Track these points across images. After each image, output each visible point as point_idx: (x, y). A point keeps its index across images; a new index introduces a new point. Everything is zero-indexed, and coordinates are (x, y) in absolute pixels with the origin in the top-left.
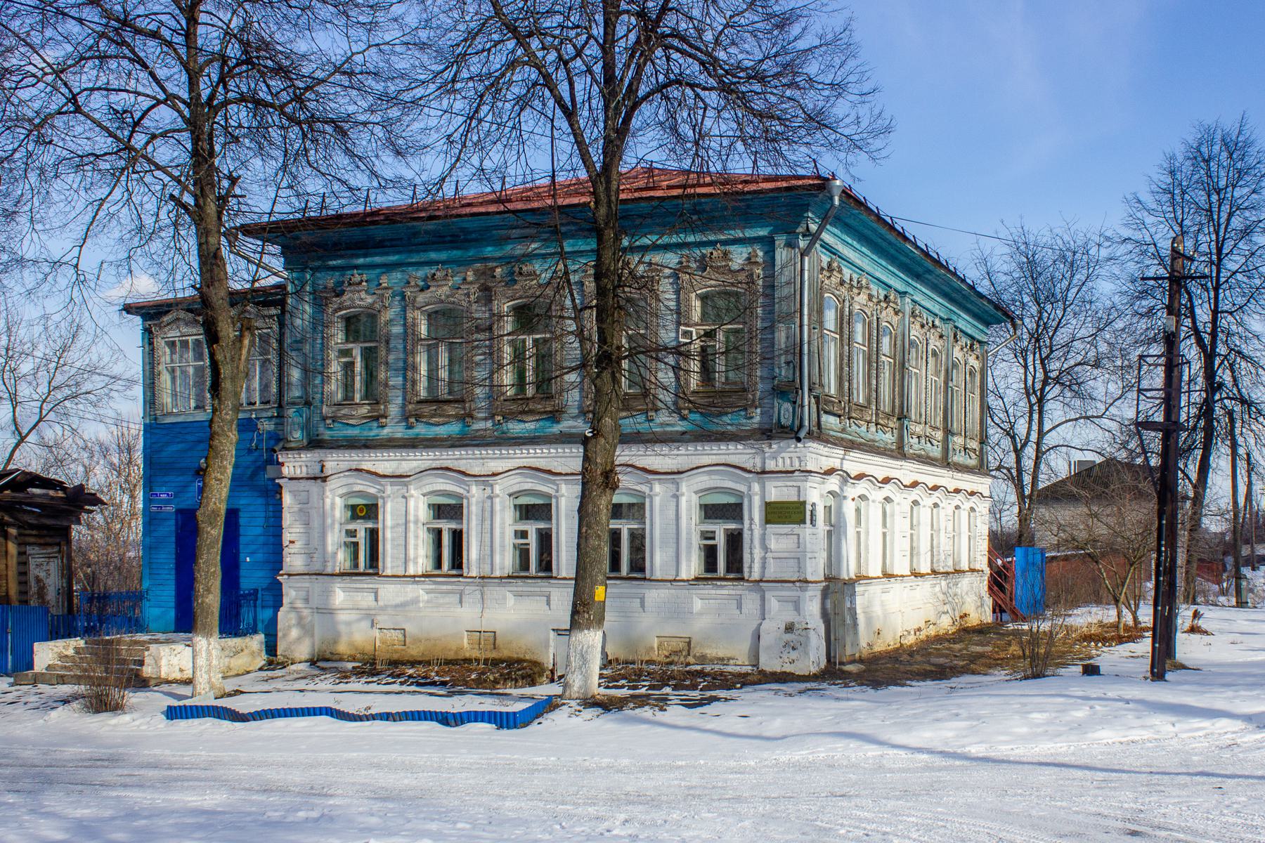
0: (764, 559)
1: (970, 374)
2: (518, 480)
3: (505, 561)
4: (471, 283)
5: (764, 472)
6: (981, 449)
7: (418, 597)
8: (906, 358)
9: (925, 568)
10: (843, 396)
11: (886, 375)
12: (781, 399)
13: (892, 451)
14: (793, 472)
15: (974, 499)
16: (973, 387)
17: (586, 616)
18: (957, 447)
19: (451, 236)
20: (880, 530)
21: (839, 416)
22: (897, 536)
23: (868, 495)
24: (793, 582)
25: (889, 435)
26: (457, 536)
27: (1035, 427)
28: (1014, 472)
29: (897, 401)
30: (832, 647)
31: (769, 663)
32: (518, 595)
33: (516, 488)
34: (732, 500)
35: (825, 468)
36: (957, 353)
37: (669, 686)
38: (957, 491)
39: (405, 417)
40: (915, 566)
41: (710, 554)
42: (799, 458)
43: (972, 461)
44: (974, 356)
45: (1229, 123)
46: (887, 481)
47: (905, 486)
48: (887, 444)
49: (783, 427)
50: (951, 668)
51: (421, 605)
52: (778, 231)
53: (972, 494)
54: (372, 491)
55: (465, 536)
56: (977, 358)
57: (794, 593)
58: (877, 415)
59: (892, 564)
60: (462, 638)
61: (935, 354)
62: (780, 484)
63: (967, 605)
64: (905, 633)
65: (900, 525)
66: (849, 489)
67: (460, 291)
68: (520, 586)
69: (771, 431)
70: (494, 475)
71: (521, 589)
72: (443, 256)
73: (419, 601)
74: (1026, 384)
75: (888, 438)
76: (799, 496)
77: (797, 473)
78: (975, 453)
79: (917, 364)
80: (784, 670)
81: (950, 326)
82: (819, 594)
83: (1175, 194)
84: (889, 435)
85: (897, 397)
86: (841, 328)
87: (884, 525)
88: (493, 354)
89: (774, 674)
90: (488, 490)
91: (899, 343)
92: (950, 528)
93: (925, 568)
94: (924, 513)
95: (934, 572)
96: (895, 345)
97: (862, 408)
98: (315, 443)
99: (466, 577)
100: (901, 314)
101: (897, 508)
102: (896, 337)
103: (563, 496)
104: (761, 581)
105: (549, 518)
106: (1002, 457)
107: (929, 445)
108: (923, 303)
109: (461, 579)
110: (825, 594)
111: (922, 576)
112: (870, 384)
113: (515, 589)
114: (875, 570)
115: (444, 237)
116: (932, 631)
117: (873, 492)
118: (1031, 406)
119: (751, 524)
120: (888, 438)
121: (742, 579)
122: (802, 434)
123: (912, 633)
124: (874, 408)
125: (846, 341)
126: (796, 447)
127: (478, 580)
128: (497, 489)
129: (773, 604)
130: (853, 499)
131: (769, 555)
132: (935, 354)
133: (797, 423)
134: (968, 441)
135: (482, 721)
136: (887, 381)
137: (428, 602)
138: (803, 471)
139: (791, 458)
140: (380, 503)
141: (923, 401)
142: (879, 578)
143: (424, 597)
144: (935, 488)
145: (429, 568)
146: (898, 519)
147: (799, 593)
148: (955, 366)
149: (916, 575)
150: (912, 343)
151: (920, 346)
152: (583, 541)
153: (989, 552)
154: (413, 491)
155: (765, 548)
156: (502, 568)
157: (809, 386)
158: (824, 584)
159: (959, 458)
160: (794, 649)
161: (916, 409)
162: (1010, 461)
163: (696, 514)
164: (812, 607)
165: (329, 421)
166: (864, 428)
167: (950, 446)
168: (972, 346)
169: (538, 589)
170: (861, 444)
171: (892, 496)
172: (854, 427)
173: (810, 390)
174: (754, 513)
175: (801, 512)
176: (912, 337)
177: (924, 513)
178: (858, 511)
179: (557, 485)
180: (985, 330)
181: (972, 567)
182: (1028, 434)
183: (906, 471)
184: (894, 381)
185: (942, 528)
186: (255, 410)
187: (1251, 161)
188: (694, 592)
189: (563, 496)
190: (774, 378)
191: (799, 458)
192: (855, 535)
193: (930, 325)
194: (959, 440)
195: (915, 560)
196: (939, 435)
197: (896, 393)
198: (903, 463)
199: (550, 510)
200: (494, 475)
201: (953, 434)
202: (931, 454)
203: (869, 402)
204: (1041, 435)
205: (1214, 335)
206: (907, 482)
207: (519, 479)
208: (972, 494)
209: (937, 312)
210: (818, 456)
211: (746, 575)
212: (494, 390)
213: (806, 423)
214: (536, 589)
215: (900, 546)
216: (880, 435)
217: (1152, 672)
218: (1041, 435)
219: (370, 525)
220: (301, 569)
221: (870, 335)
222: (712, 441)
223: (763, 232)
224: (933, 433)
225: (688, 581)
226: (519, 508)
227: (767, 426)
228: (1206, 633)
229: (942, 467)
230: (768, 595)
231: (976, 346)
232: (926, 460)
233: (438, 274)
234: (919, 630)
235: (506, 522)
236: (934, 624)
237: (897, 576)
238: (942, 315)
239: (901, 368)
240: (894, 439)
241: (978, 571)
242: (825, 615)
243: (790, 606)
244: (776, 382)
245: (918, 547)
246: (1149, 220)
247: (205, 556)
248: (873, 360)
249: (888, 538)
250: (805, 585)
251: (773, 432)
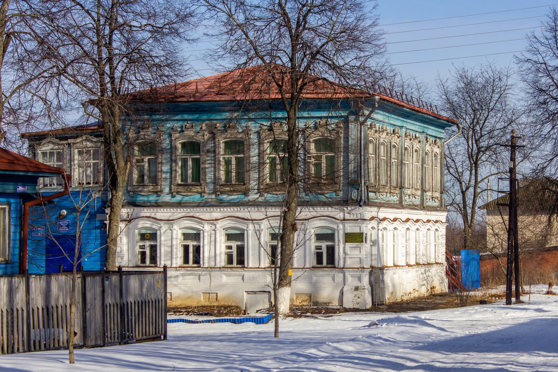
0: (345, 258)
1: (435, 156)
2: (228, 222)
3: (222, 261)
4: (205, 130)
5: (344, 220)
8: (403, 158)
9: (413, 262)
10: (377, 183)
11: (394, 168)
12: (353, 187)
13: (397, 204)
14: (357, 220)
15: (437, 224)
16: (436, 163)
17: (285, 281)
18: (428, 198)
19: (195, 108)
20: (392, 244)
21: (375, 192)
22: (400, 246)
23: (387, 228)
24: (358, 268)
25: (395, 197)
27: (473, 177)
28: (461, 206)
29: (399, 180)
30: (374, 298)
31: (347, 304)
33: (228, 226)
34: (330, 232)
36: (428, 148)
37: (309, 312)
38: (429, 221)
39: (171, 192)
40: (408, 261)
41: (319, 256)
42: (360, 213)
43: (436, 204)
44: (437, 147)
46: (395, 220)
47: (403, 222)
48: (394, 201)
49: (353, 200)
50: (427, 308)
53: (437, 222)
54: (154, 227)
55: (201, 249)
56: (438, 147)
57: (358, 273)
58: (390, 188)
59: (397, 260)
60: (200, 297)
61: (416, 151)
63: (434, 281)
64: (404, 294)
65: (401, 241)
67: (199, 134)
68: (229, 272)
69: (348, 201)
70: (216, 220)
71: (229, 273)
74: (468, 151)
75: (395, 199)
76: (360, 230)
77: (359, 220)
79: (408, 159)
80: (354, 307)
81: (424, 135)
82: (368, 273)
84: (395, 197)
85: (399, 178)
86: (376, 152)
87: (394, 242)
89: (350, 309)
90: (213, 227)
91: (400, 151)
92: (425, 241)
93: (413, 262)
94: (412, 234)
95: (418, 264)
96: (398, 153)
97: (384, 186)
98: (133, 204)
99: (202, 268)
100: (400, 138)
101: (399, 232)
102: (398, 149)
103: (250, 230)
104: (343, 268)
105: (243, 240)
107: (414, 198)
108: (411, 128)
109: (200, 269)
110: (371, 274)
111: (411, 266)
112: (387, 174)
113: (227, 273)
114: (390, 264)
115: (192, 108)
116: (416, 295)
117: (389, 226)
118: (471, 164)
119: (339, 243)
121: (335, 267)
122: (362, 204)
123: (407, 294)
124: (389, 185)
125: (377, 156)
126: (359, 209)
127: (209, 269)
128: (218, 226)
129: (349, 279)
130: (381, 230)
131: (347, 256)
132: (416, 151)
133: (359, 198)
135: (249, 321)
136: (394, 171)
138: (362, 220)
139: (357, 214)
140: (158, 233)
141: (411, 178)
142: (392, 267)
144: (417, 221)
145: (182, 264)
146: (400, 237)
147: (360, 273)
148: (426, 154)
149: (409, 266)
150: (406, 149)
151: (409, 149)
152: (283, 252)
153: (446, 253)
154: (175, 227)
157: (364, 182)
158: (371, 269)
159: (430, 203)
160: (359, 298)
161: (408, 181)
162: (459, 198)
164: (366, 280)
165: (131, 193)
166: (385, 196)
167: (425, 198)
168: (435, 141)
169: (238, 273)
170: (384, 203)
171: (397, 227)
172: (381, 196)
173: (365, 184)
174: (340, 237)
175: (361, 238)
176: (406, 146)
178: (383, 235)
179: (248, 225)
181: (429, 262)
183: (403, 214)
184: (398, 170)
185: (421, 241)
186: (91, 187)
188: (312, 273)
189: (250, 230)
190: (349, 178)
191: (360, 213)
193: (414, 137)
194: (429, 194)
195: (408, 258)
196: (419, 193)
197: (399, 176)
199: (244, 236)
200: (216, 220)
201: (426, 192)
202: (415, 203)
203: (387, 183)
206: (404, 220)
207: (229, 222)
208: (437, 222)
209: (417, 130)
210: (369, 212)
211: (336, 266)
213: (363, 198)
214: (237, 273)
215: (401, 251)
216: (392, 198)
217: (506, 303)
220: (170, 262)
221: (387, 151)
222: (321, 206)
223: (344, 114)
224: (416, 193)
225: (310, 268)
227: (345, 199)
228: (554, 294)
229: (422, 210)
230: (346, 274)
231: (438, 140)
232: (413, 207)
233: (188, 125)
234: (410, 293)
236: (418, 291)
237: (400, 266)
238: (420, 131)
239: (401, 164)
240: (398, 199)
241: (440, 264)
242: (370, 283)
243: (357, 279)
244: (350, 180)
246: (542, 49)
247: (111, 259)
248: (389, 164)
249: (395, 247)
250: (363, 269)
251: (345, 202)
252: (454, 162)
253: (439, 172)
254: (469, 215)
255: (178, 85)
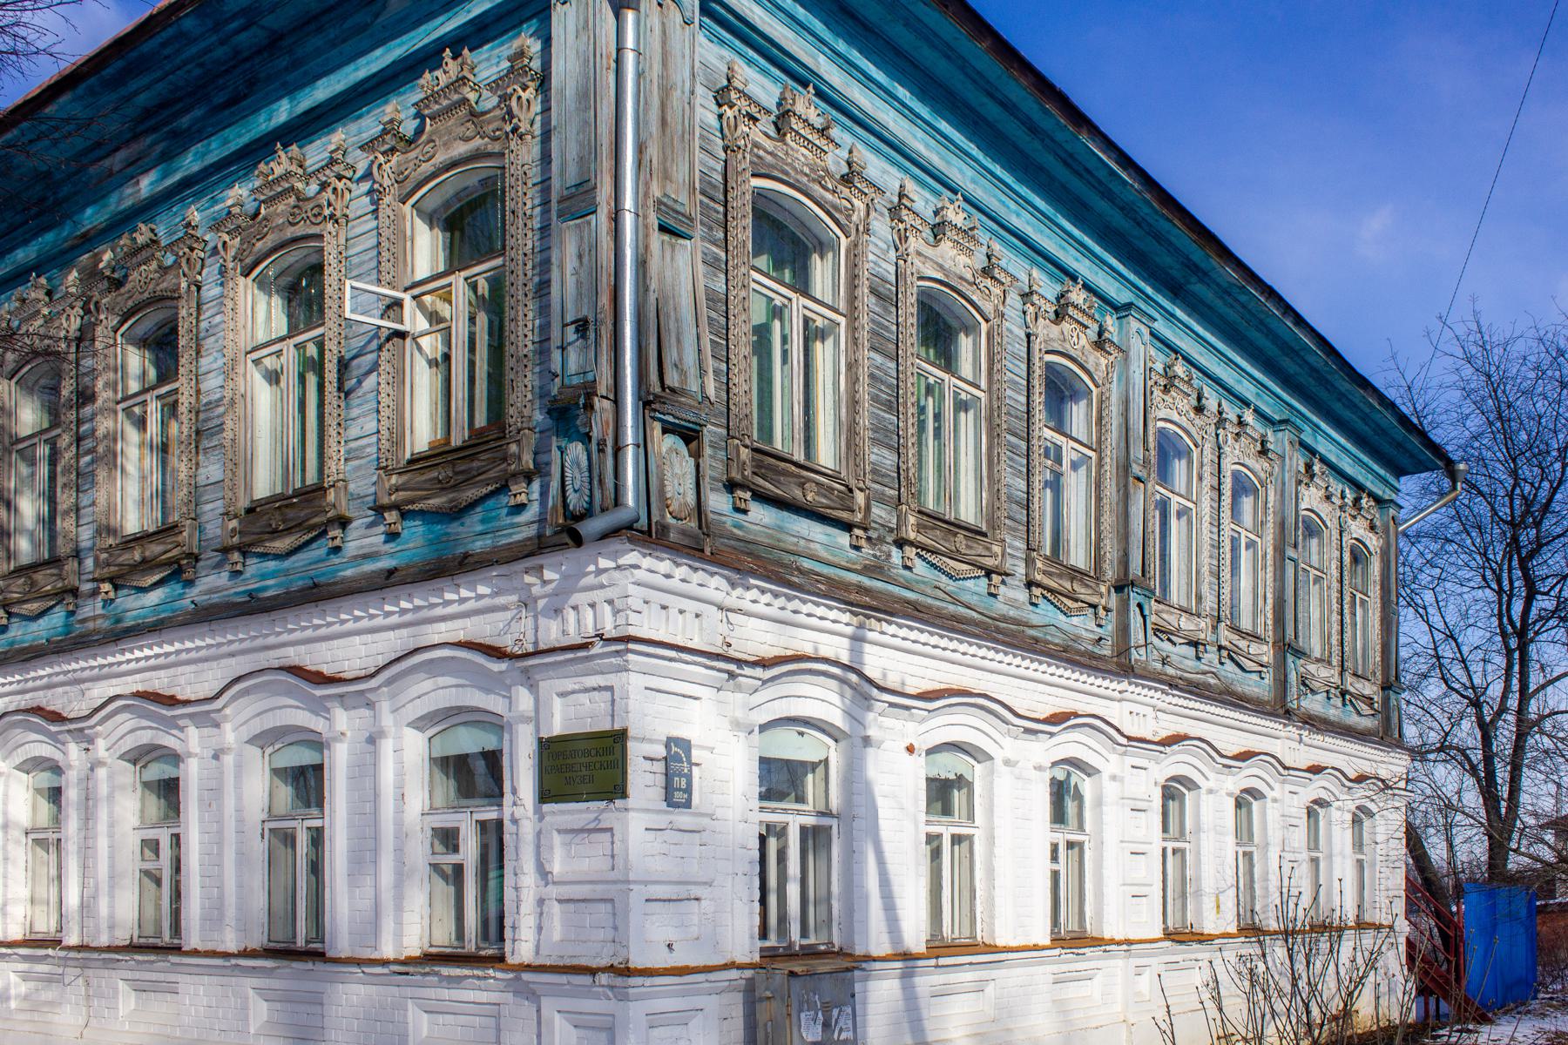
6: (1386, 701)
7: (7, 988)
23: (1196, 776)
24: (592, 972)
32: (140, 988)
35: (1164, 734)
38: (1316, 770)
42: (610, 602)
51: (13, 1004)
62: (569, 684)
66: (887, 722)
73: (8, 999)
78: (1371, 705)
91: (1114, 409)
94: (1337, 824)
101: (1111, 790)
106: (1447, 729)
117: (1007, 742)
134: (1349, 679)
137: (26, 998)
143: (19, 987)
155: (544, 874)
156: (215, 915)
158: (748, 973)
177: (1337, 824)
180: (1392, 480)
182: (1504, 697)
188: (409, 991)
192: (925, 850)
198: (1124, 685)
204: (1525, 696)
218: (1525, 696)
237: (1112, 942)
245: (1199, 879)
252: (1455, 640)
253: (1378, 614)
254: (1504, 792)
255: (368, 273)
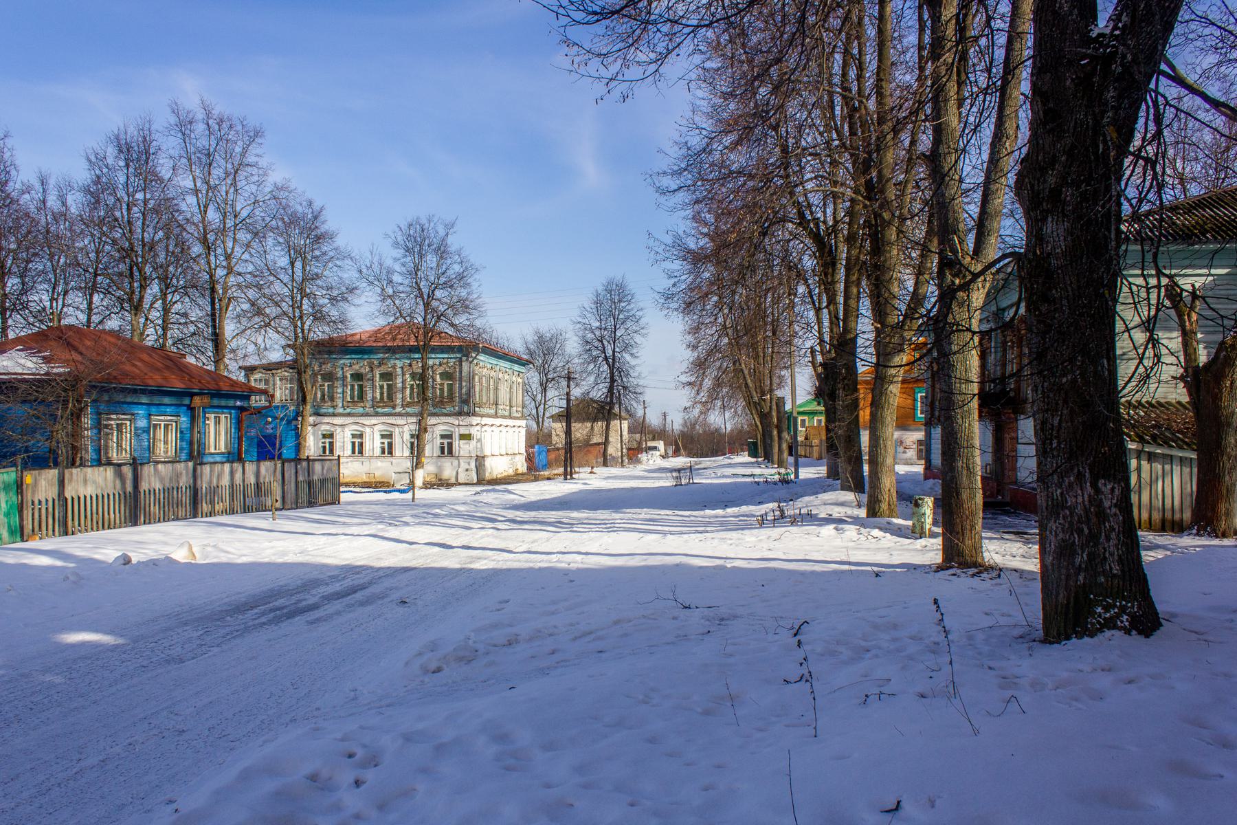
3: (378, 452)
11: (492, 391)
26: (361, 444)
38: (514, 426)
39: (343, 407)
41: (442, 449)
43: (520, 415)
45: (619, 278)
52: (464, 355)
72: (357, 357)
83: (598, 303)
88: (373, 387)
95: (507, 454)
98: (317, 414)
120: (492, 412)
129: (462, 464)
159: (515, 415)
162: (534, 412)
163: (379, 437)
174: (456, 436)
183: (498, 421)
187: (627, 292)
196: (508, 408)
205: (613, 360)
212: (374, 398)
219: (389, 440)
226: (352, 434)
232: (504, 417)
235: (378, 440)
239: (496, 389)
246: (588, 315)
248: (488, 389)
251: (460, 414)
